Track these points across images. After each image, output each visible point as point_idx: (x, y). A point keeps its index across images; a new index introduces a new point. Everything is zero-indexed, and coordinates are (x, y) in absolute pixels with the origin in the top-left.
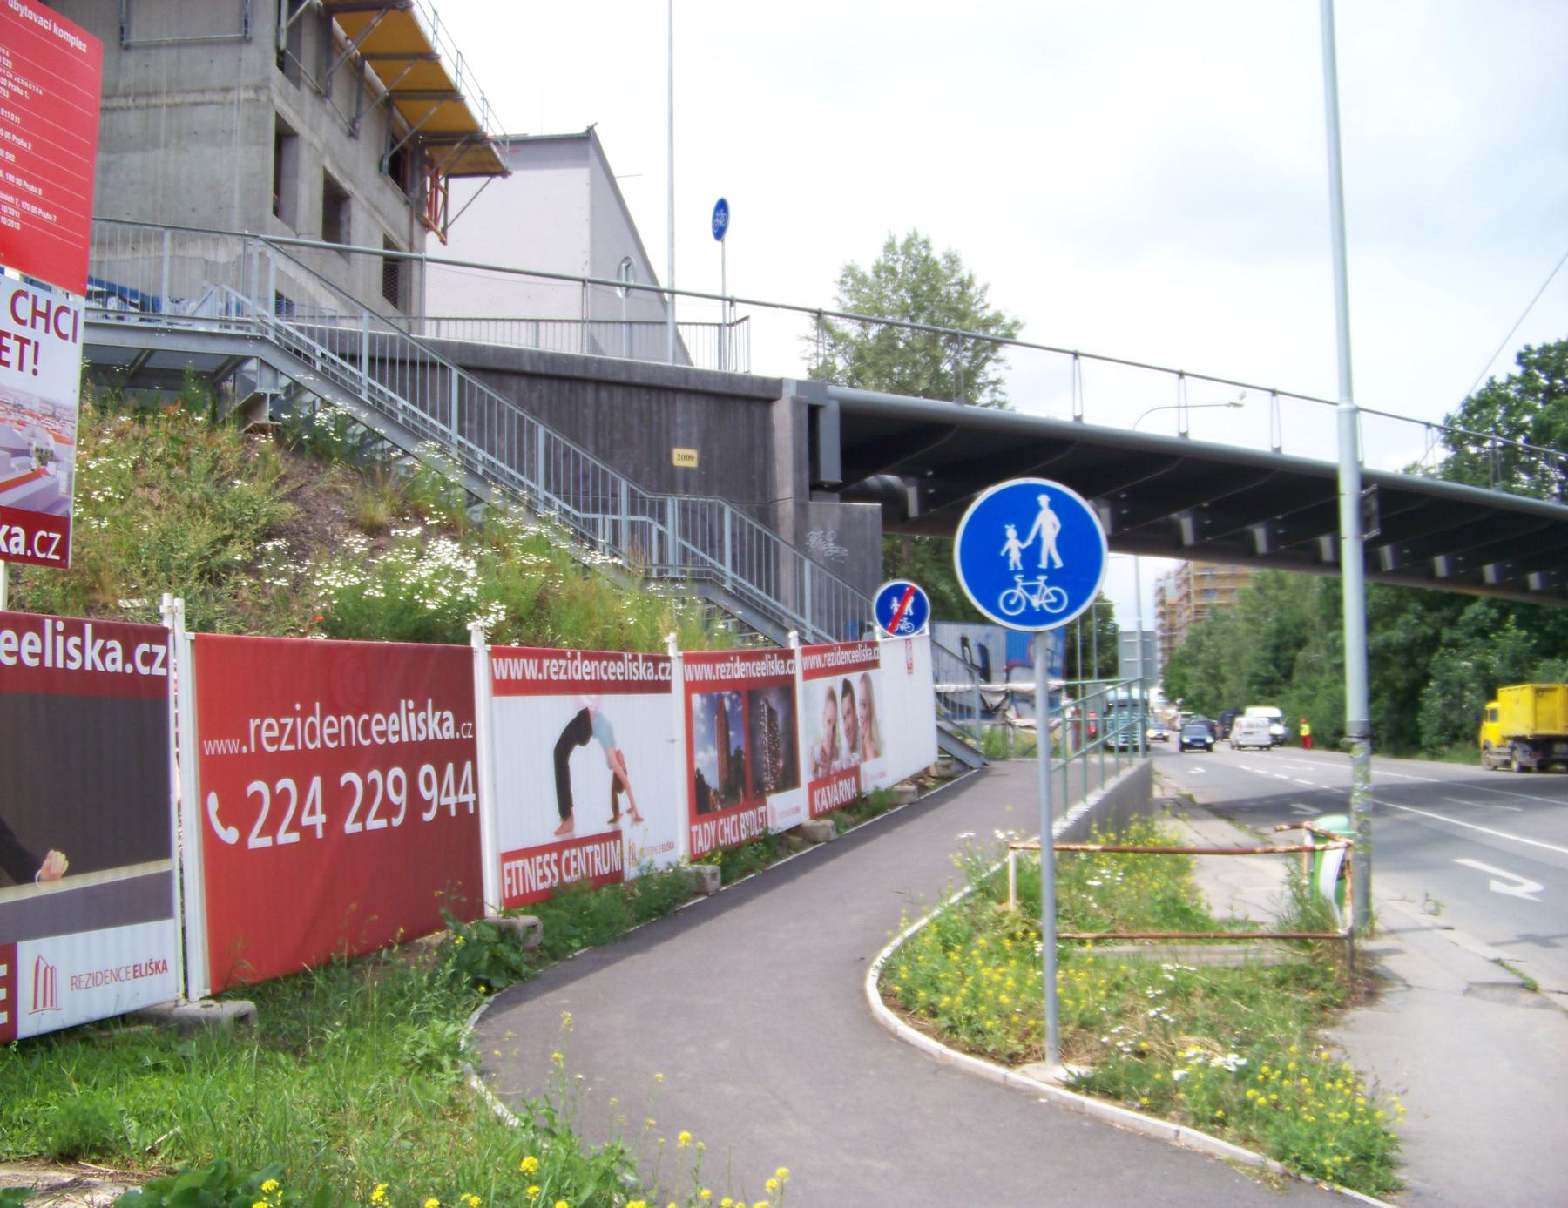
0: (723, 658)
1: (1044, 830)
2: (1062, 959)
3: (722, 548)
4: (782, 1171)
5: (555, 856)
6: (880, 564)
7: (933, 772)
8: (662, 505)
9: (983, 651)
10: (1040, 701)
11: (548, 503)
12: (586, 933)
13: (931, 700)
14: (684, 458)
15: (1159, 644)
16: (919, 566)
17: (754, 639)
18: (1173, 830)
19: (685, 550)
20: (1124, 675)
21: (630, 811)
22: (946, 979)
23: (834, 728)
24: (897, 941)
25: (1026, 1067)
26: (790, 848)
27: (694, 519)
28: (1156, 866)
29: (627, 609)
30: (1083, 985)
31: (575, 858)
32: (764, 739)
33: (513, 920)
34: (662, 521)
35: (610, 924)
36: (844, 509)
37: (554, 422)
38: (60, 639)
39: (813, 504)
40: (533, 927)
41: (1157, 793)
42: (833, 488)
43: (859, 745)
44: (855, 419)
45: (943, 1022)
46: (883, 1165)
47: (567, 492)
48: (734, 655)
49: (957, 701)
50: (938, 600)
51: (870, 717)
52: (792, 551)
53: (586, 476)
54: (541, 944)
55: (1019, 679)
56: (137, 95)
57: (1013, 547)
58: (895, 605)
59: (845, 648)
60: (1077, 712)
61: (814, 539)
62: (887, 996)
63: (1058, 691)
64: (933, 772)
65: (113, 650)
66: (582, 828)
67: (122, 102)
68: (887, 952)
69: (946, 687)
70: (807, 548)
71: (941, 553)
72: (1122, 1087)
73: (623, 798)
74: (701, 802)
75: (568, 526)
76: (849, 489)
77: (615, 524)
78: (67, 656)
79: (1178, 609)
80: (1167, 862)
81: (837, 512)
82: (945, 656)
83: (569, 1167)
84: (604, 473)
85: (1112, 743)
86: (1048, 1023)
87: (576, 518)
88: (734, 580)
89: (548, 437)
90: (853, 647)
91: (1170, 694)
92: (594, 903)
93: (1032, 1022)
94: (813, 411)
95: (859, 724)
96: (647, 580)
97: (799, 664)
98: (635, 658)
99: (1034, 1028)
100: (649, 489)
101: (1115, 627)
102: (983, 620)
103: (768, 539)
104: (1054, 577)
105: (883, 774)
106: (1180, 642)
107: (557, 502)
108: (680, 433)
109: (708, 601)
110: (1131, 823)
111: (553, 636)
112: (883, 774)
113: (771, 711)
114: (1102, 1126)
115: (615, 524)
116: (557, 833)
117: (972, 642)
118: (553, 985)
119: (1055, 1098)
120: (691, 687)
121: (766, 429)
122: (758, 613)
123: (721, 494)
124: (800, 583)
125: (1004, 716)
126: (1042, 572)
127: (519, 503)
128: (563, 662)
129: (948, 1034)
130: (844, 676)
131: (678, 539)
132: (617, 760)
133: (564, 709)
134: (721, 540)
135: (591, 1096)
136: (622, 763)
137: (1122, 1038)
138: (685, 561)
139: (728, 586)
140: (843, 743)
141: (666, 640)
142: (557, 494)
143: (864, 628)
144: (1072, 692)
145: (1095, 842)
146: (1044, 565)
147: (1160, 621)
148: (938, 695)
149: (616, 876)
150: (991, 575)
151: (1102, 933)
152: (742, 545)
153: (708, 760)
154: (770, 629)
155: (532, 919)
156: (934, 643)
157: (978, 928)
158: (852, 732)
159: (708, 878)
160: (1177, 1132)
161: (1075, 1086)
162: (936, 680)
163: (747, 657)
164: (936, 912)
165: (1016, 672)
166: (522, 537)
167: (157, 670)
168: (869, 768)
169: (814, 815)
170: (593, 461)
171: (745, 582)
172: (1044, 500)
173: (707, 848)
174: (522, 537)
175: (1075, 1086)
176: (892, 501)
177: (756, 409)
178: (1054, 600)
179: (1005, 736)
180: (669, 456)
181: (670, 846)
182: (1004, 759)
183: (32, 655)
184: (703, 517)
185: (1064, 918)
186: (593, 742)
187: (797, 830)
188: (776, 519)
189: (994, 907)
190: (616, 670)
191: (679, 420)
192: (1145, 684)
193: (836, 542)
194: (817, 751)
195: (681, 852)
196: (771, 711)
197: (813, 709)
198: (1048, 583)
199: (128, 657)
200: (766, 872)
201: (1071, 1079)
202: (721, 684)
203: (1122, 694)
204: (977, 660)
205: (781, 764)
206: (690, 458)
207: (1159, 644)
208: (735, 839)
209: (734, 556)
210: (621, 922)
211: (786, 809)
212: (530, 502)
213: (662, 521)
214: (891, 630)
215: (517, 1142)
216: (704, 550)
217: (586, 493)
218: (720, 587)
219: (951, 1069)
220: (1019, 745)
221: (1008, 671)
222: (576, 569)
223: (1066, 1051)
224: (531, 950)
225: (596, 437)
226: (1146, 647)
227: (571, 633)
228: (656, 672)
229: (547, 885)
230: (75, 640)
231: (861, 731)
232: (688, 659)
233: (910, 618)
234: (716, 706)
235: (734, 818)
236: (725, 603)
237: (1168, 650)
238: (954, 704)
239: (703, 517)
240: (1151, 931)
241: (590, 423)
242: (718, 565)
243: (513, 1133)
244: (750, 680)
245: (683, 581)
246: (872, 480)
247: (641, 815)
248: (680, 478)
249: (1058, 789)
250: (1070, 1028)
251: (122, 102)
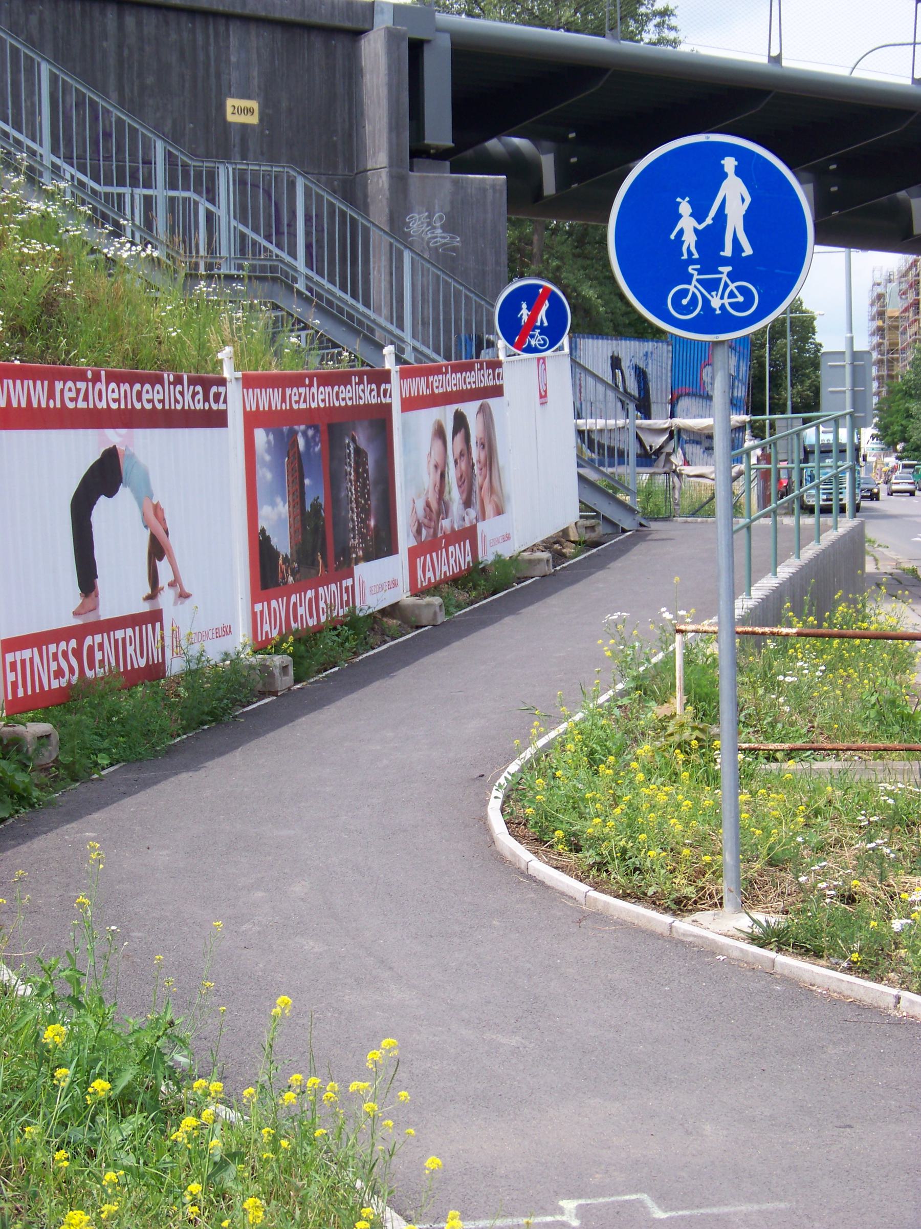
0: (297, 381)
1: (723, 605)
2: (744, 776)
3: (293, 235)
4: (387, 1042)
5: (73, 643)
6: (504, 259)
7: (574, 536)
8: (212, 176)
9: (641, 375)
10: (720, 443)
11: (56, 171)
12: (116, 746)
13: (572, 439)
14: (241, 111)
15: (874, 371)
16: (555, 263)
17: (336, 358)
18: (890, 614)
19: (243, 236)
20: (827, 410)
21: (171, 585)
22: (594, 800)
23: (442, 476)
24: (528, 754)
25: (697, 916)
26: (385, 635)
27: (255, 197)
28: (868, 658)
29: (166, 316)
30: (776, 810)
31: (101, 647)
32: (350, 490)
33: (20, 728)
34: (212, 200)
35: (148, 734)
36: (456, 183)
37: (60, 58)
38: (172, 387)
39: (415, 176)
40: (44, 738)
41: (870, 567)
42: (441, 155)
43: (476, 499)
44: (469, 56)
45: (589, 857)
46: (515, 1041)
47: (81, 157)
48: (311, 378)
49: (605, 441)
50: (582, 309)
51: (490, 460)
52: (387, 239)
53: (107, 135)
54: (56, 760)
55: (688, 415)
57: (688, 226)
58: (525, 313)
59: (456, 369)
60: (765, 457)
61: (416, 224)
62: (514, 825)
63: (741, 428)
64: (574, 536)
66: (108, 609)
68: (514, 767)
69: (588, 423)
70: (408, 235)
71: (589, 247)
72: (824, 941)
73: (163, 566)
74: (268, 572)
75: (83, 203)
76: (462, 156)
77: (148, 202)
79: (903, 324)
80: (883, 652)
81: (448, 187)
82: (591, 381)
83: (99, 1046)
84: (133, 131)
85: (811, 502)
86: (728, 858)
87: (94, 191)
88: (308, 278)
89: (54, 79)
90: (469, 368)
91: (889, 437)
92: (126, 704)
93: (707, 858)
94: (416, 48)
95: (476, 470)
96: (192, 277)
97: (396, 391)
98: (178, 381)
99: (709, 865)
100: (194, 154)
101: (818, 346)
102: (642, 331)
103: (353, 221)
104: (741, 268)
105: (507, 537)
106: (904, 369)
107: (69, 170)
108: (235, 76)
109: (276, 307)
110: (837, 604)
111: (68, 353)
112: (507, 537)
113: (358, 451)
114: (800, 991)
115: (148, 202)
116: (76, 614)
117: (625, 364)
118: (72, 815)
119: (736, 954)
120: (252, 420)
121: (353, 72)
122: (343, 323)
123: (292, 161)
124: (399, 282)
125: (668, 461)
126: (725, 262)
127: (17, 171)
128: (81, 385)
129: (597, 873)
130: (455, 407)
131: (234, 223)
132: (154, 518)
133: (82, 448)
134: (292, 224)
135: (126, 956)
136: (162, 521)
137: (827, 876)
138: (243, 251)
139: (300, 286)
140: (455, 495)
141: (220, 356)
142: (69, 159)
143: (482, 344)
144: (758, 432)
145: (790, 626)
147: (876, 339)
148: (580, 433)
149: (155, 671)
150: (658, 266)
151: (799, 743)
152: (320, 231)
153: (276, 516)
154: (357, 345)
155: (45, 727)
156: (575, 363)
157: (635, 737)
158: (467, 482)
159: (277, 672)
160: (898, 999)
161: (763, 938)
162: (578, 416)
163: (327, 380)
164: (578, 717)
165: (684, 403)
166: (20, 217)
168: (488, 529)
169: (416, 592)
170: (116, 113)
171: (324, 282)
172: (729, 164)
173: (275, 633)
174: (20, 217)
175: (763, 938)
176: (520, 172)
177: (339, 45)
178: (741, 299)
179: (670, 489)
180: (221, 108)
181: (227, 631)
182: (666, 519)
184: (268, 193)
185: (746, 725)
186: (124, 492)
187: (393, 610)
188: (366, 196)
189: (656, 711)
190: (153, 397)
191: (233, 59)
192: (856, 425)
193: (444, 228)
194: (420, 506)
195: (241, 636)
196: (358, 451)
197: (415, 450)
198: (732, 277)
200: (352, 665)
201: (757, 931)
202: (292, 416)
203: (827, 438)
204: (633, 387)
205: (372, 523)
206: (250, 111)
207: (874, 371)
208: (312, 622)
209: (308, 246)
210: (163, 731)
211: (380, 582)
212: (30, 168)
213: (212, 200)
214: (518, 346)
215: (30, 1017)
216: (268, 238)
217: (108, 158)
218: (290, 288)
219: (600, 917)
220: (685, 503)
221: (673, 403)
222: (97, 262)
223: (750, 895)
224: (45, 769)
225: (120, 78)
226: (858, 374)
227: (91, 348)
228: (206, 399)
229: (64, 682)
230: (179, 388)
231: (478, 480)
232: (249, 382)
233: (543, 331)
234: (285, 445)
235: (310, 594)
236: (297, 309)
237: (888, 379)
238: (601, 446)
239: (268, 193)
240: (860, 743)
241: (112, 61)
242: (288, 259)
243: (24, 1005)
244: (331, 410)
245: (239, 279)
246: (494, 145)
247: (187, 590)
248: (235, 139)
249: (741, 556)
250: (757, 866)
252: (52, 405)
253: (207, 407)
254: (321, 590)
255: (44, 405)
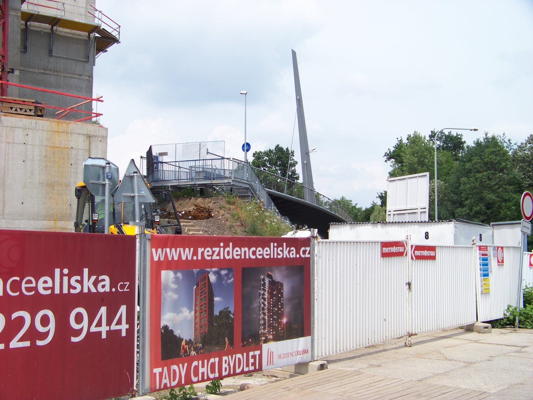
38: (276, 249)
56: (54, 71)
65: (293, 250)
67: (49, 72)
78: (278, 254)
146: (27, 344)
167: (307, 256)
183: (267, 255)
199: (298, 252)
230: (281, 248)
251: (49, 72)
252: (195, 258)
253: (298, 256)
254: (225, 358)
255: (190, 258)
